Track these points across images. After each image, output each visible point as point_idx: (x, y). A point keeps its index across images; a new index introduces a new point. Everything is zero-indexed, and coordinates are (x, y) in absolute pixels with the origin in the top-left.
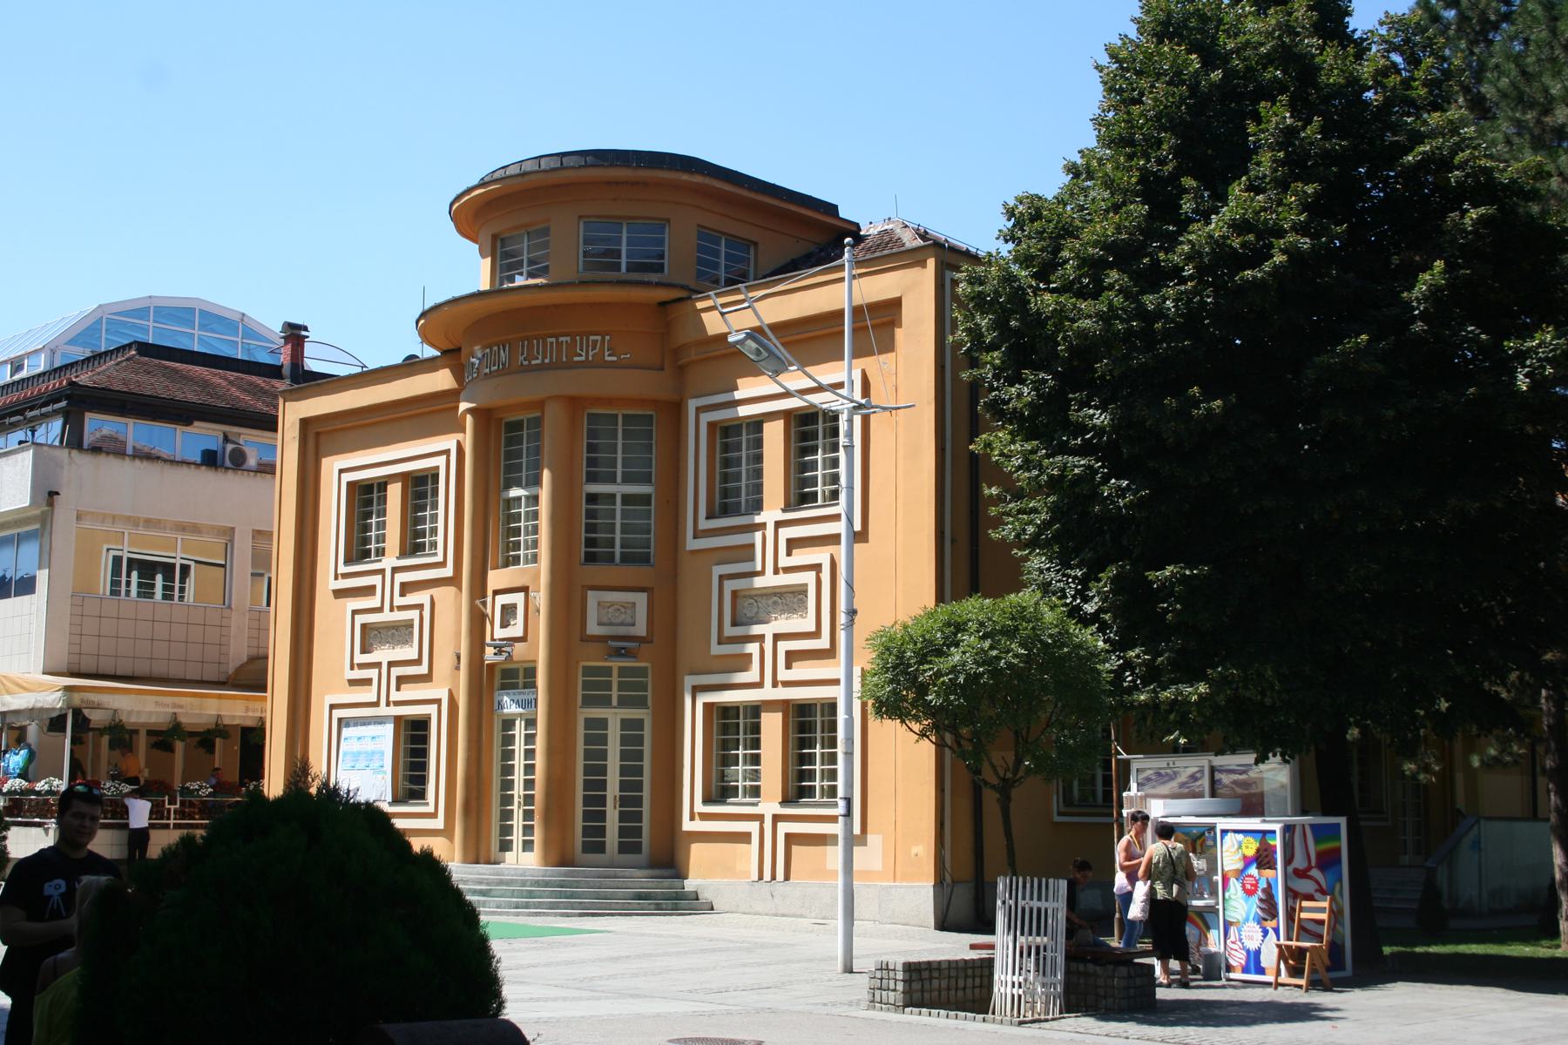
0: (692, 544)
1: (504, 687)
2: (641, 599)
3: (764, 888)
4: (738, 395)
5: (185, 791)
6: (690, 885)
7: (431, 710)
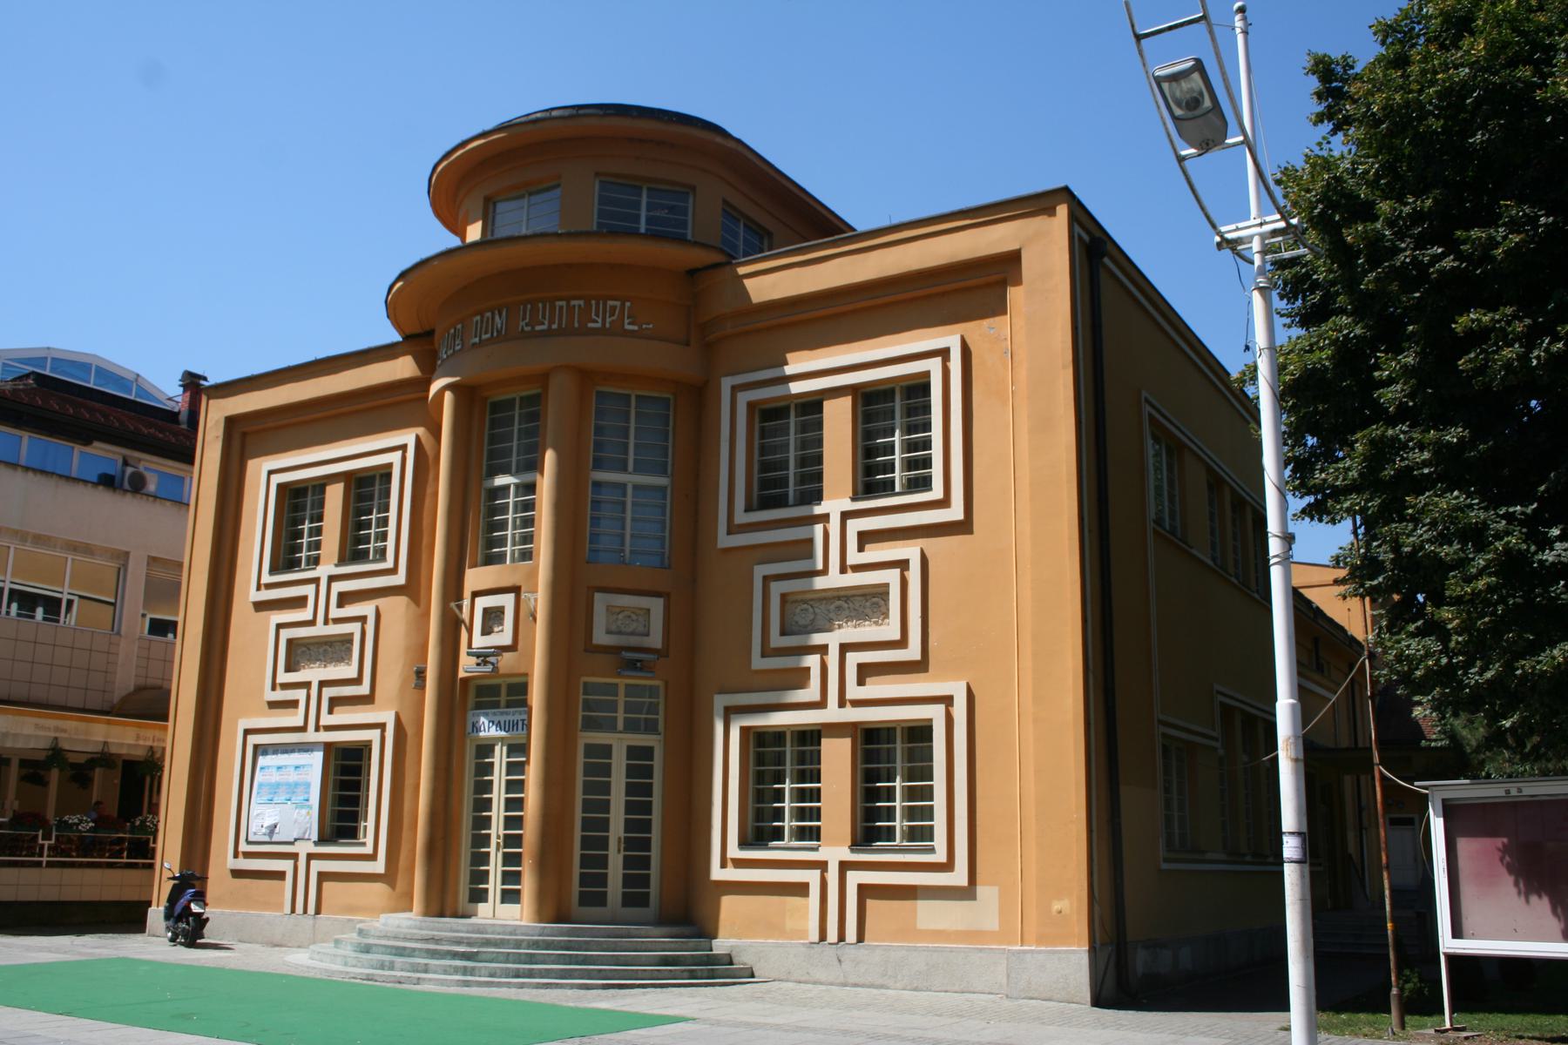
0: (725, 541)
1: (479, 706)
2: (656, 606)
3: (828, 952)
4: (789, 370)
5: (62, 825)
6: (720, 945)
7: (373, 735)
